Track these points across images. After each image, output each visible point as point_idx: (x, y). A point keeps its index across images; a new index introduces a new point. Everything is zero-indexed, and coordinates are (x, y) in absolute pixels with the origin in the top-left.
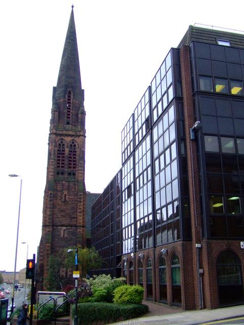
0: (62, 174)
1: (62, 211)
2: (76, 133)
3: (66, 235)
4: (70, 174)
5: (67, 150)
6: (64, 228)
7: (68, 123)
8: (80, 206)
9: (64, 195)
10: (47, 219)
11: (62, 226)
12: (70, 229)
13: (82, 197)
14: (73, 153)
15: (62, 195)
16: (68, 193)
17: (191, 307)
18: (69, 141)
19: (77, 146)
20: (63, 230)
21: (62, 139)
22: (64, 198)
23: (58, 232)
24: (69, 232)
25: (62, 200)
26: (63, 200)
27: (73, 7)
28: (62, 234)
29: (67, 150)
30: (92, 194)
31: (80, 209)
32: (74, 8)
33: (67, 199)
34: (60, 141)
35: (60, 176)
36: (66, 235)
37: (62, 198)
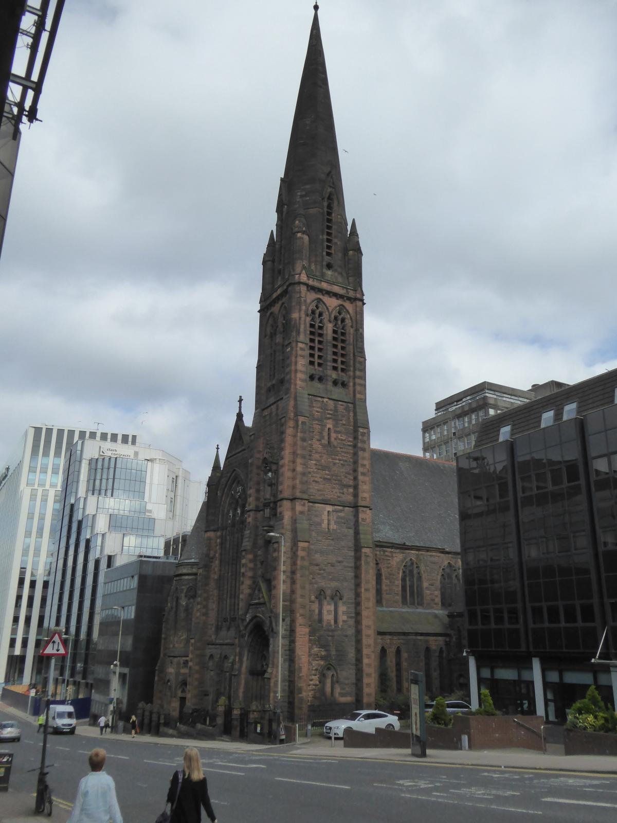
0: (320, 379)
1: (324, 468)
2: (348, 292)
3: (333, 526)
4: (335, 383)
5: (329, 328)
6: (329, 508)
7: (329, 266)
8: (363, 458)
9: (327, 429)
10: (298, 482)
11: (325, 502)
12: (341, 511)
13: (544, 605)
14: (340, 336)
15: (323, 430)
16: (334, 426)
17: (243, 736)
18: (333, 306)
19: (348, 322)
20: (326, 513)
21: (319, 300)
22: (326, 438)
23: (316, 516)
24: (338, 517)
25: (323, 441)
26: (325, 441)
27: (316, 7)
28: (326, 522)
29: (329, 328)
30: (32, 104)
31: (363, 466)
32: (319, 12)
33: (332, 439)
34: (314, 304)
35: (316, 384)
36: (333, 526)
37: (323, 437)
